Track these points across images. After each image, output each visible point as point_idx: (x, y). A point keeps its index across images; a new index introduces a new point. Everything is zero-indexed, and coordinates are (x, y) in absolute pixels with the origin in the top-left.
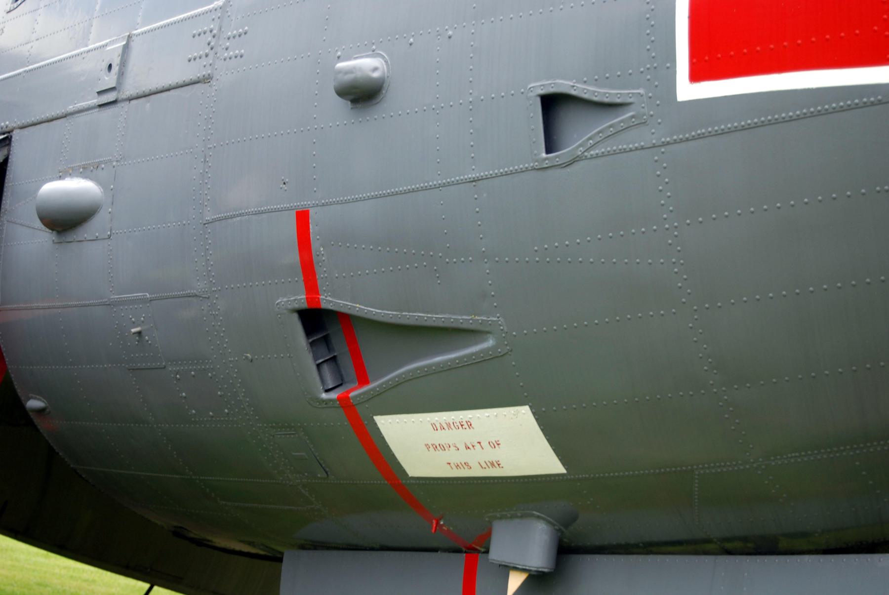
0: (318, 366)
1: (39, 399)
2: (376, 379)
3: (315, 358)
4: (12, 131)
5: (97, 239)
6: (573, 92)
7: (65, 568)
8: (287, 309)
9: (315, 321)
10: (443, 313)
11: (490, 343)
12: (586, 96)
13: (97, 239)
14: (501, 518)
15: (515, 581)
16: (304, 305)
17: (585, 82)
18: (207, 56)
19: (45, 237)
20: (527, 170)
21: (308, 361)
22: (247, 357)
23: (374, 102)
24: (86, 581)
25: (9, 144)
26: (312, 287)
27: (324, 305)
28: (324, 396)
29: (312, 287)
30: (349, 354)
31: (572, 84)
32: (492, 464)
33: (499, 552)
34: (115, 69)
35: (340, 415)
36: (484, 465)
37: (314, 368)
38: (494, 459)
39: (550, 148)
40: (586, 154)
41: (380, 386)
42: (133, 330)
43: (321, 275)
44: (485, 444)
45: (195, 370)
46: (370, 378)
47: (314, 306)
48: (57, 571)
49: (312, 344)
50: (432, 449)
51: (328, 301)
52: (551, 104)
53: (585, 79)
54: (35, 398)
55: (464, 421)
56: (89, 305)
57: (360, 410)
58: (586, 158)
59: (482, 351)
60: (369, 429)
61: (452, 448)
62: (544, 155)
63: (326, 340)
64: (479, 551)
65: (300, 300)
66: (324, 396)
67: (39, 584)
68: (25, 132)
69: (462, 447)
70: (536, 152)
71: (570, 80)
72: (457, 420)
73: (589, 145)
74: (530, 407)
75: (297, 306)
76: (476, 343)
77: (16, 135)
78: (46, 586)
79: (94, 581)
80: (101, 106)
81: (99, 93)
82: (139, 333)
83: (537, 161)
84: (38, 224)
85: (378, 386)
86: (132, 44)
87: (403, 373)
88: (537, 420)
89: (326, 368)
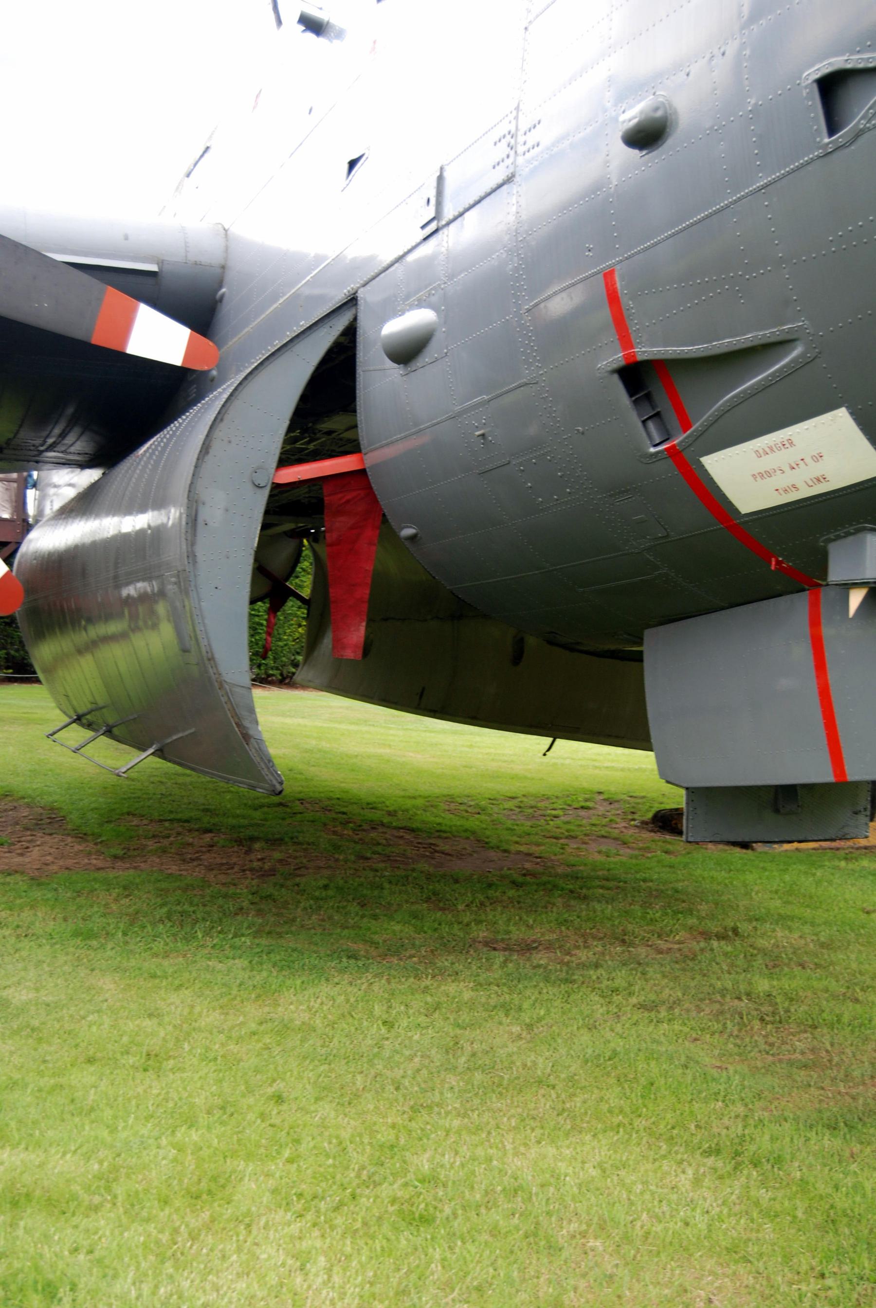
0: (644, 422)
1: (411, 527)
2: (698, 421)
3: (640, 415)
4: (356, 292)
5: (437, 360)
6: (849, 66)
7: (487, 754)
8: (607, 372)
9: (636, 377)
10: (749, 332)
11: (797, 352)
12: (861, 66)
13: (437, 360)
14: (838, 538)
15: (856, 598)
16: (622, 363)
17: (859, 52)
18: (508, 156)
19: (395, 371)
20: (812, 160)
21: (634, 418)
22: (578, 430)
23: (660, 142)
24: (505, 761)
25: (356, 304)
26: (625, 340)
27: (640, 358)
28: (652, 450)
29: (625, 340)
30: (673, 411)
31: (846, 58)
32: (819, 480)
33: (836, 574)
34: (433, 201)
35: (669, 467)
36: (811, 483)
37: (640, 424)
38: (818, 474)
39: (832, 129)
40: (868, 125)
41: (701, 425)
42: (477, 433)
43: (633, 327)
44: (808, 460)
45: (535, 458)
46: (691, 420)
47: (632, 360)
48: (480, 756)
49: (635, 402)
50: (759, 479)
51: (644, 351)
52: (831, 87)
53: (858, 49)
54: (408, 527)
55: (785, 440)
56: (438, 423)
57: (686, 455)
58: (869, 129)
59: (792, 361)
60: (704, 481)
61: (778, 472)
62: (827, 140)
63: (648, 397)
64: (821, 585)
65: (617, 358)
66: (652, 450)
67: (466, 767)
68: (368, 287)
69: (786, 468)
70: (818, 139)
71: (843, 54)
72: (778, 441)
73: (870, 115)
74: (847, 407)
75: (615, 366)
76: (786, 356)
77: (360, 294)
78: (471, 767)
79: (512, 761)
80: (425, 239)
81: (423, 227)
82: (483, 435)
83: (820, 149)
84: (389, 364)
85: (700, 426)
86: (445, 174)
87: (721, 406)
88: (855, 419)
89: (651, 425)
